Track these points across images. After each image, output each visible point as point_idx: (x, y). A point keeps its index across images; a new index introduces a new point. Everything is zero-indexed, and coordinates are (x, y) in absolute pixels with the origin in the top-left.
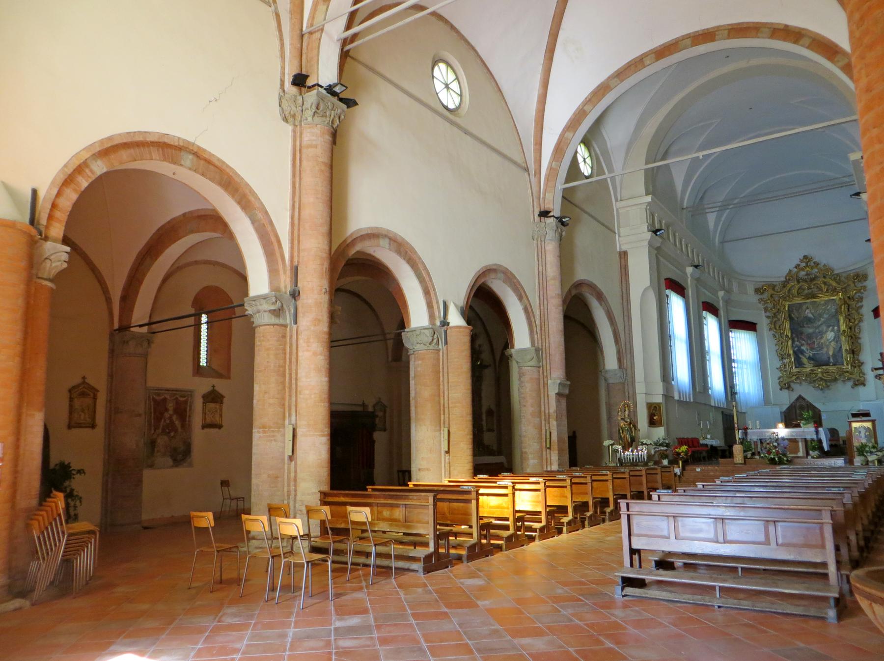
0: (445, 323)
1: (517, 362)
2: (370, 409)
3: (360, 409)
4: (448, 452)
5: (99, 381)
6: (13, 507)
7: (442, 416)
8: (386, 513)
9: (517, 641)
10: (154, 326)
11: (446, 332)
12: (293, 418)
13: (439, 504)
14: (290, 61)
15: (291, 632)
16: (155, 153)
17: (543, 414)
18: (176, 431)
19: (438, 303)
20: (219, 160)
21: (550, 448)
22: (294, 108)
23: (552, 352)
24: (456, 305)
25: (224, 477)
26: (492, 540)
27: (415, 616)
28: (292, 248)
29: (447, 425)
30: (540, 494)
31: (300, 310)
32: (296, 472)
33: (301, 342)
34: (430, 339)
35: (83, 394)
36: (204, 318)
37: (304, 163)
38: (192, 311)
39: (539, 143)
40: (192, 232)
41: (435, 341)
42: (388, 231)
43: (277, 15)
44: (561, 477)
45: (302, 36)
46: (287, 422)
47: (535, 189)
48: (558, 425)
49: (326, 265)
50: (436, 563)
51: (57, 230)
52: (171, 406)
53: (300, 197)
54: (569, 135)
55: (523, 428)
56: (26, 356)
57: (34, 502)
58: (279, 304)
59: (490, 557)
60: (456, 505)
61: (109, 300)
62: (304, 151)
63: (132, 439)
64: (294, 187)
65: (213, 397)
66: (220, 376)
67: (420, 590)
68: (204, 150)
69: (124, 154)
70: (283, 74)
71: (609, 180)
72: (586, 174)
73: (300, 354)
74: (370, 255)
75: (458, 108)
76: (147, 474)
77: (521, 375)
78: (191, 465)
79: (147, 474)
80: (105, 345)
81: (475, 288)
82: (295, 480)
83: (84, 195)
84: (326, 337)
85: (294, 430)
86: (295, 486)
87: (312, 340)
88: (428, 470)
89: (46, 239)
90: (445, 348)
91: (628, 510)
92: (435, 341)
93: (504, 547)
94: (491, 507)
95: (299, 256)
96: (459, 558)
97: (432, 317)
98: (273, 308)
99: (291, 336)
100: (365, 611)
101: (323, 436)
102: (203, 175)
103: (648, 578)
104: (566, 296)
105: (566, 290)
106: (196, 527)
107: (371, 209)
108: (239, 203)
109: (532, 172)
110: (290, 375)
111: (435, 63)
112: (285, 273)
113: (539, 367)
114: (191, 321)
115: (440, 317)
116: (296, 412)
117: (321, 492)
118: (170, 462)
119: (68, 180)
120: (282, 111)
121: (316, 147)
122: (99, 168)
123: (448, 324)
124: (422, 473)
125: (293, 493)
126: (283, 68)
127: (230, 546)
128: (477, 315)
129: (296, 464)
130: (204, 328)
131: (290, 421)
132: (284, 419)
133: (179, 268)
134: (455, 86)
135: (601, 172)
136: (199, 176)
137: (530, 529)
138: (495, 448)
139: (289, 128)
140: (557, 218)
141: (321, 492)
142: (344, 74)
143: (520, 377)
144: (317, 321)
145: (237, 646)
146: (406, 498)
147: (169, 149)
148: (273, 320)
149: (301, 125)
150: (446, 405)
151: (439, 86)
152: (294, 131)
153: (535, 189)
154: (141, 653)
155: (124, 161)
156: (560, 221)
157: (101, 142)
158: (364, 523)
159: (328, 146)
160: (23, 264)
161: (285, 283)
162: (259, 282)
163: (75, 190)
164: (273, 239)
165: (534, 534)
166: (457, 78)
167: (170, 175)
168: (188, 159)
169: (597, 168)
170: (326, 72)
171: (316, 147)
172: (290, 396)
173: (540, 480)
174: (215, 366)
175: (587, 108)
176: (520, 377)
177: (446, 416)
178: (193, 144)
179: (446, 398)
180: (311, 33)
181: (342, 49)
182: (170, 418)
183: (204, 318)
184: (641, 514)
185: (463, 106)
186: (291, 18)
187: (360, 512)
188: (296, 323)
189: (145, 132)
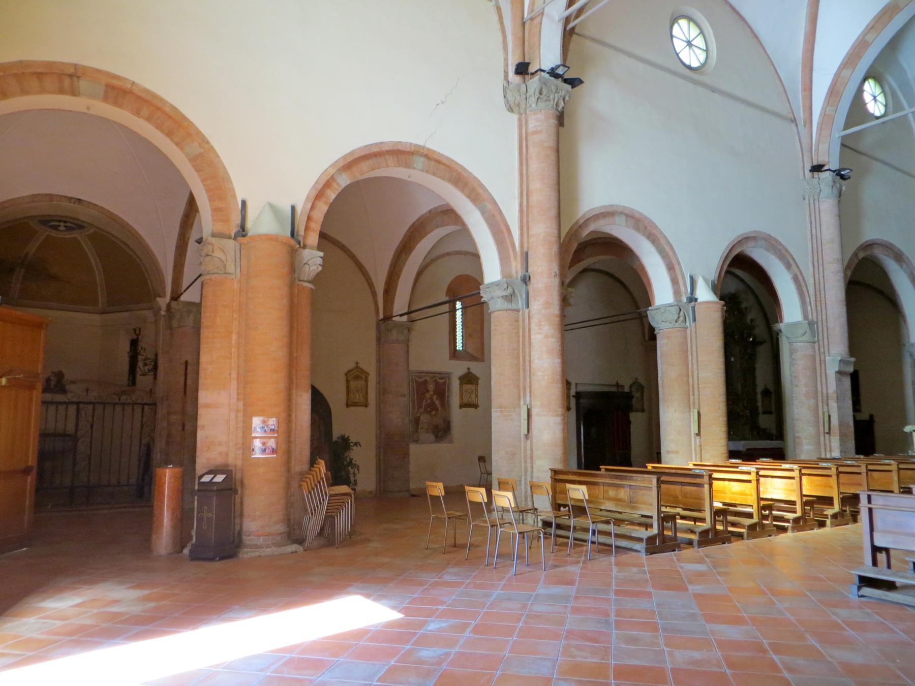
0: (692, 299)
1: (787, 338)
2: (627, 390)
3: (614, 389)
4: (698, 434)
5: (370, 367)
6: (288, 470)
7: (692, 397)
8: (612, 493)
9: (709, 627)
10: (413, 315)
11: (693, 308)
12: (528, 398)
13: (663, 486)
14: (513, 51)
15: (497, 593)
16: (391, 160)
17: (819, 395)
18: (437, 410)
19: (683, 278)
20: (448, 158)
21: (829, 433)
22: (518, 97)
23: (831, 324)
24: (705, 280)
25: (481, 454)
26: (724, 527)
27: (617, 592)
28: (522, 234)
29: (697, 406)
30: (795, 482)
31: (531, 294)
32: (531, 450)
33: (533, 325)
34: (676, 317)
35: (357, 377)
36: (459, 305)
37: (531, 150)
38: (447, 299)
39: (808, 88)
40: (437, 227)
41: (682, 318)
42: (624, 207)
43: (499, 9)
44: (825, 465)
45: (524, 24)
46: (522, 402)
47: (805, 141)
48: (839, 408)
49: (555, 248)
50: (660, 545)
51: (313, 239)
52: (431, 387)
53: (527, 184)
54: (846, 73)
55: (796, 411)
56: (292, 346)
57: (306, 467)
58: (510, 290)
59: (726, 545)
60: (689, 488)
61: (374, 294)
62: (530, 138)
63: (398, 417)
64: (521, 175)
65: (469, 379)
66: (473, 358)
67: (634, 569)
68: (434, 152)
69: (364, 165)
70: (506, 65)
71: (910, 116)
72: (877, 114)
73: (532, 337)
74: (606, 233)
75: (703, 65)
76: (414, 448)
77: (792, 352)
78: (451, 442)
79: (414, 448)
80: (373, 333)
81: (730, 259)
82: (532, 458)
83: (333, 206)
84: (558, 319)
85: (529, 411)
86: (532, 463)
87: (543, 323)
88: (677, 452)
89: (305, 247)
90: (693, 325)
91: (869, 502)
92: (682, 318)
93: (745, 536)
94: (733, 493)
95: (528, 242)
96: (690, 543)
97: (677, 293)
98: (505, 294)
99: (524, 320)
100: (571, 583)
101: (557, 416)
102: (434, 174)
103: (899, 581)
104: (851, 260)
105: (849, 255)
106: (470, 502)
107: (607, 186)
108: (469, 197)
109: (801, 122)
110: (524, 357)
111: (674, 21)
112: (515, 259)
113: (814, 343)
114: (446, 308)
115: (686, 293)
116: (530, 392)
117: (552, 470)
118: (432, 437)
119: (319, 195)
120: (507, 102)
121: (540, 132)
122: (344, 181)
123: (696, 300)
124: (672, 455)
125: (529, 469)
126: (506, 60)
127: (459, 514)
128: (748, 286)
129: (531, 442)
130: (459, 314)
131: (525, 401)
132: (519, 399)
133: (433, 261)
134: (699, 42)
135: (898, 107)
136: (430, 176)
137: (781, 519)
138: (774, 432)
139: (515, 117)
140: (834, 171)
141: (552, 470)
142: (570, 54)
143: (791, 354)
144: (548, 304)
145: (445, 599)
146: (630, 479)
147: (401, 154)
148: (506, 305)
149: (526, 113)
150: (696, 386)
151: (679, 45)
152: (520, 120)
153: (805, 141)
154: (368, 596)
155: (365, 171)
156: (840, 175)
157: (344, 157)
158: (582, 501)
159: (553, 129)
160: (286, 270)
161: (516, 267)
162: (492, 271)
163: (326, 203)
164: (503, 227)
165: (786, 524)
166: (702, 32)
167: (406, 178)
168: (420, 162)
169: (892, 104)
170: (549, 55)
171: (540, 132)
172: (525, 378)
173: (795, 467)
174: (470, 350)
175: (869, 38)
176: (791, 354)
177: (696, 397)
178: (424, 147)
179: (695, 378)
180: (532, 19)
181: (565, 29)
182: (431, 398)
183: (459, 305)
184: (885, 507)
185: (709, 61)
186: (512, 8)
187: (578, 490)
188: (528, 307)
189: (381, 143)
